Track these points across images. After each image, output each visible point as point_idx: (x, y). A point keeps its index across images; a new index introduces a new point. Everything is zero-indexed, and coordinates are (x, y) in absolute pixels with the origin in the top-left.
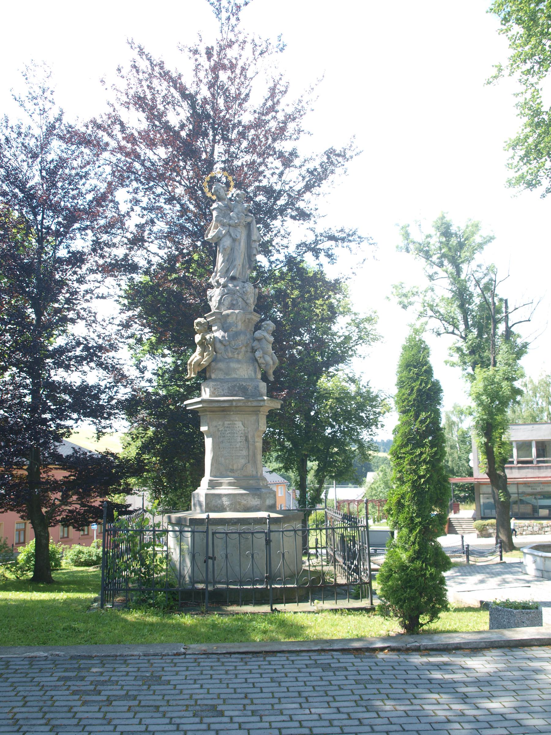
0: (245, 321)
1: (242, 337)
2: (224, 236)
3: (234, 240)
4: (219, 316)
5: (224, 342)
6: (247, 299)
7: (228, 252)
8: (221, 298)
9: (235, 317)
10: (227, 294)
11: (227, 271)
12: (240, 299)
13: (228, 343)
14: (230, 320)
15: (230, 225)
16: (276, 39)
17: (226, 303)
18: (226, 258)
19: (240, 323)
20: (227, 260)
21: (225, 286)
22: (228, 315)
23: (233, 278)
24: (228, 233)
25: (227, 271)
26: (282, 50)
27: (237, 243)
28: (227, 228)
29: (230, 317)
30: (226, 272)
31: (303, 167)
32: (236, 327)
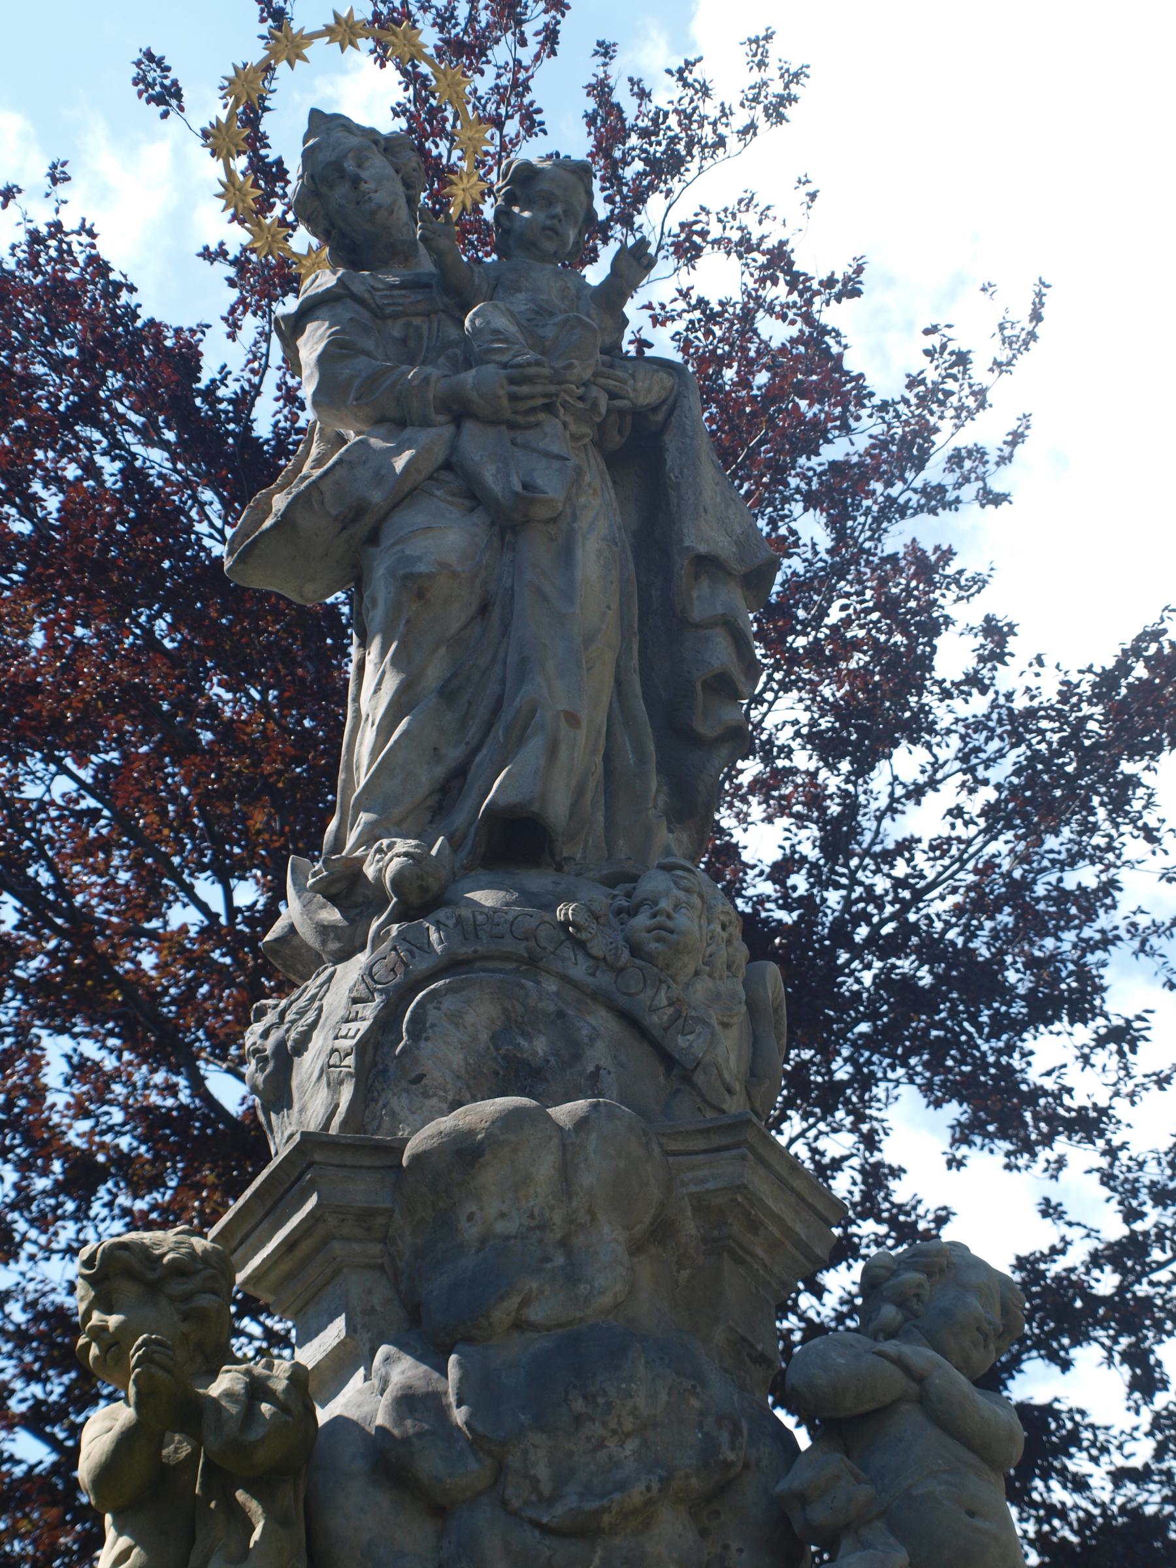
0: (663, 1230)
1: (643, 1391)
2: (408, 492)
3: (508, 521)
4: (363, 1190)
5: (430, 1464)
6: (681, 1019)
7: (457, 616)
8: (386, 1024)
9: (545, 1168)
10: (451, 966)
11: (453, 786)
12: (601, 1020)
13: (476, 1470)
14: (491, 1209)
15: (459, 411)
16: (742, 54)
17: (444, 1056)
18: (434, 673)
19: (609, 1237)
20: (448, 693)
21: (419, 897)
22: (465, 1151)
23: (515, 842)
24: (452, 474)
25: (453, 786)
26: (776, 112)
27: (537, 550)
28: (437, 436)
29: (490, 1176)
30: (433, 794)
31: (930, 796)
32: (572, 1276)
